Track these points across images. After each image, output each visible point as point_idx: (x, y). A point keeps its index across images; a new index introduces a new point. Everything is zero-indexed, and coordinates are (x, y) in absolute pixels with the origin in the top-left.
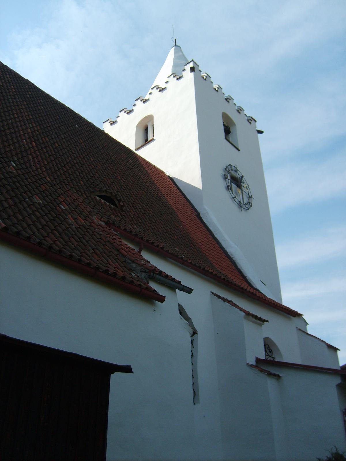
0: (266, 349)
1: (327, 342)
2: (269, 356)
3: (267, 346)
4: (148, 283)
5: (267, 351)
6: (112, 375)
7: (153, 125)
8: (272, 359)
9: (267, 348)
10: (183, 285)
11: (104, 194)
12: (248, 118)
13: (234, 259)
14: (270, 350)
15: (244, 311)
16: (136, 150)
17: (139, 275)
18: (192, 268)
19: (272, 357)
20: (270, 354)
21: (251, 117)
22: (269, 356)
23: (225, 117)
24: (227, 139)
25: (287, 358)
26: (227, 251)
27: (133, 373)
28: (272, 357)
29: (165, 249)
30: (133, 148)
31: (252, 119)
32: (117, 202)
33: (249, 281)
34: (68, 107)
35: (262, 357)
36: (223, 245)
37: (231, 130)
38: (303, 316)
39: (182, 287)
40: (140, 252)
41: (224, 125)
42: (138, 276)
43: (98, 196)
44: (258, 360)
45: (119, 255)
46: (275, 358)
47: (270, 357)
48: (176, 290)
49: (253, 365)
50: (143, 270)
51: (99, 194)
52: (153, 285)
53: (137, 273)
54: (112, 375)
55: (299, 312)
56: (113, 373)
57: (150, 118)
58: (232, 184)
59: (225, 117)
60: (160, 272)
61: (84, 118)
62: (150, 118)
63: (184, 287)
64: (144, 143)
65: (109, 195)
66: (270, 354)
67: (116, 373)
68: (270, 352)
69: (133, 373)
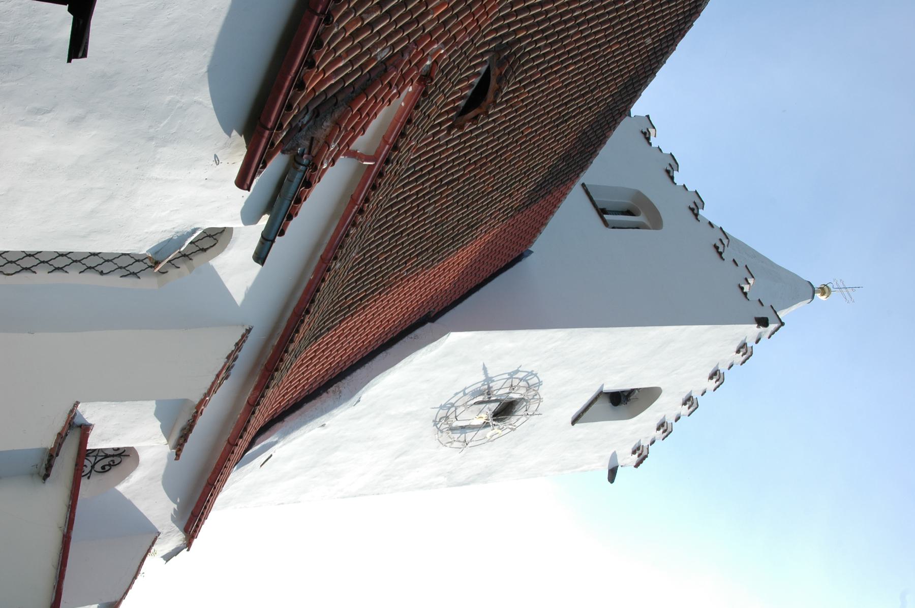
0: (111, 458)
1: (124, 602)
2: (95, 464)
3: (117, 460)
4: (283, 152)
5: (106, 461)
6: (66, 7)
7: (638, 228)
8: (87, 470)
9: (113, 461)
10: (273, 241)
11: (493, 83)
12: (645, 450)
13: (325, 394)
14: (107, 468)
15: (203, 402)
16: (583, 185)
17: (303, 133)
18: (311, 282)
19: (90, 472)
20: (98, 467)
21: (646, 456)
22: (95, 464)
23: (650, 395)
24: (601, 394)
25: (86, 487)
26: (344, 381)
27: (69, 61)
28: (90, 472)
29: (360, 219)
30: (589, 176)
31: (642, 457)
32: (471, 114)
33: (272, 428)
34: (692, 25)
35: (93, 443)
36: (358, 371)
37: (622, 408)
38: (185, 550)
39: (271, 238)
40: (353, 154)
41: (633, 391)
42: (301, 130)
43: (488, 71)
44: (85, 429)
45: (353, 92)
46: (89, 478)
47: (93, 467)
48: (265, 220)
49: (73, 418)
50: (315, 142)
51: (492, 73)
52: (278, 162)
53: (309, 128)
54: (66, 7)
55: (195, 542)
56: (70, 10)
57: (656, 222)
58: (497, 404)
59: (650, 395)
60: (308, 184)
61: (665, 62)
62: (656, 222)
63: (269, 243)
64: (600, 206)
65: (490, 96)
66: (98, 467)
67: (71, 17)
68: (103, 468)
69: (69, 61)
